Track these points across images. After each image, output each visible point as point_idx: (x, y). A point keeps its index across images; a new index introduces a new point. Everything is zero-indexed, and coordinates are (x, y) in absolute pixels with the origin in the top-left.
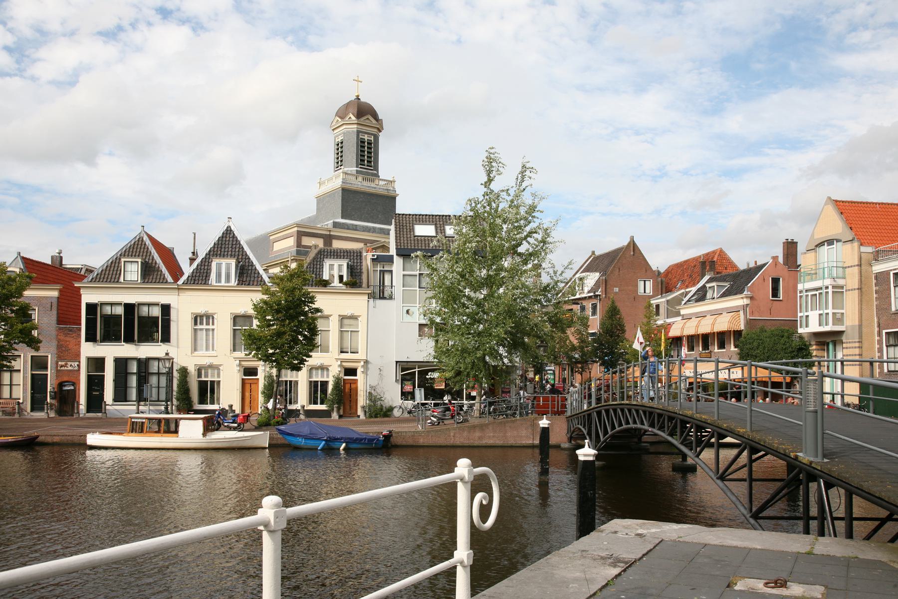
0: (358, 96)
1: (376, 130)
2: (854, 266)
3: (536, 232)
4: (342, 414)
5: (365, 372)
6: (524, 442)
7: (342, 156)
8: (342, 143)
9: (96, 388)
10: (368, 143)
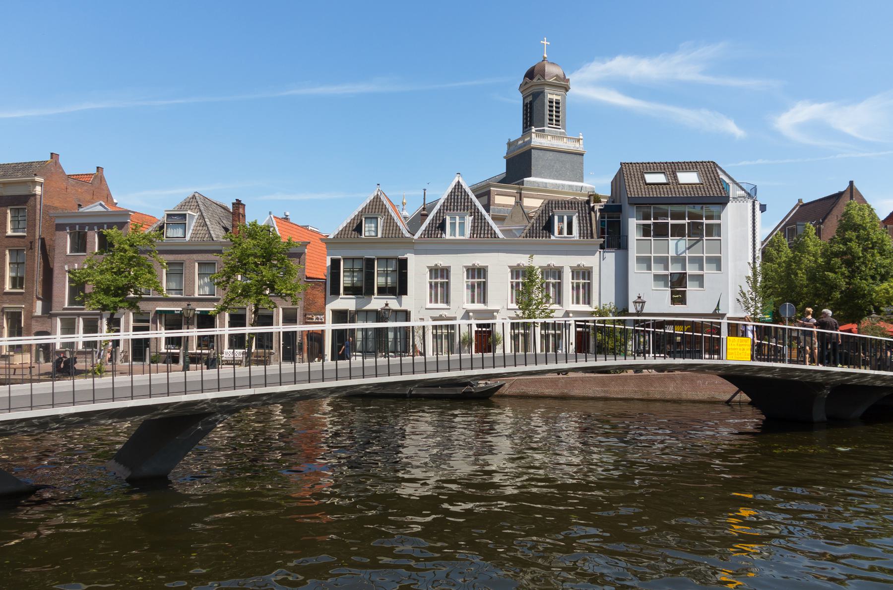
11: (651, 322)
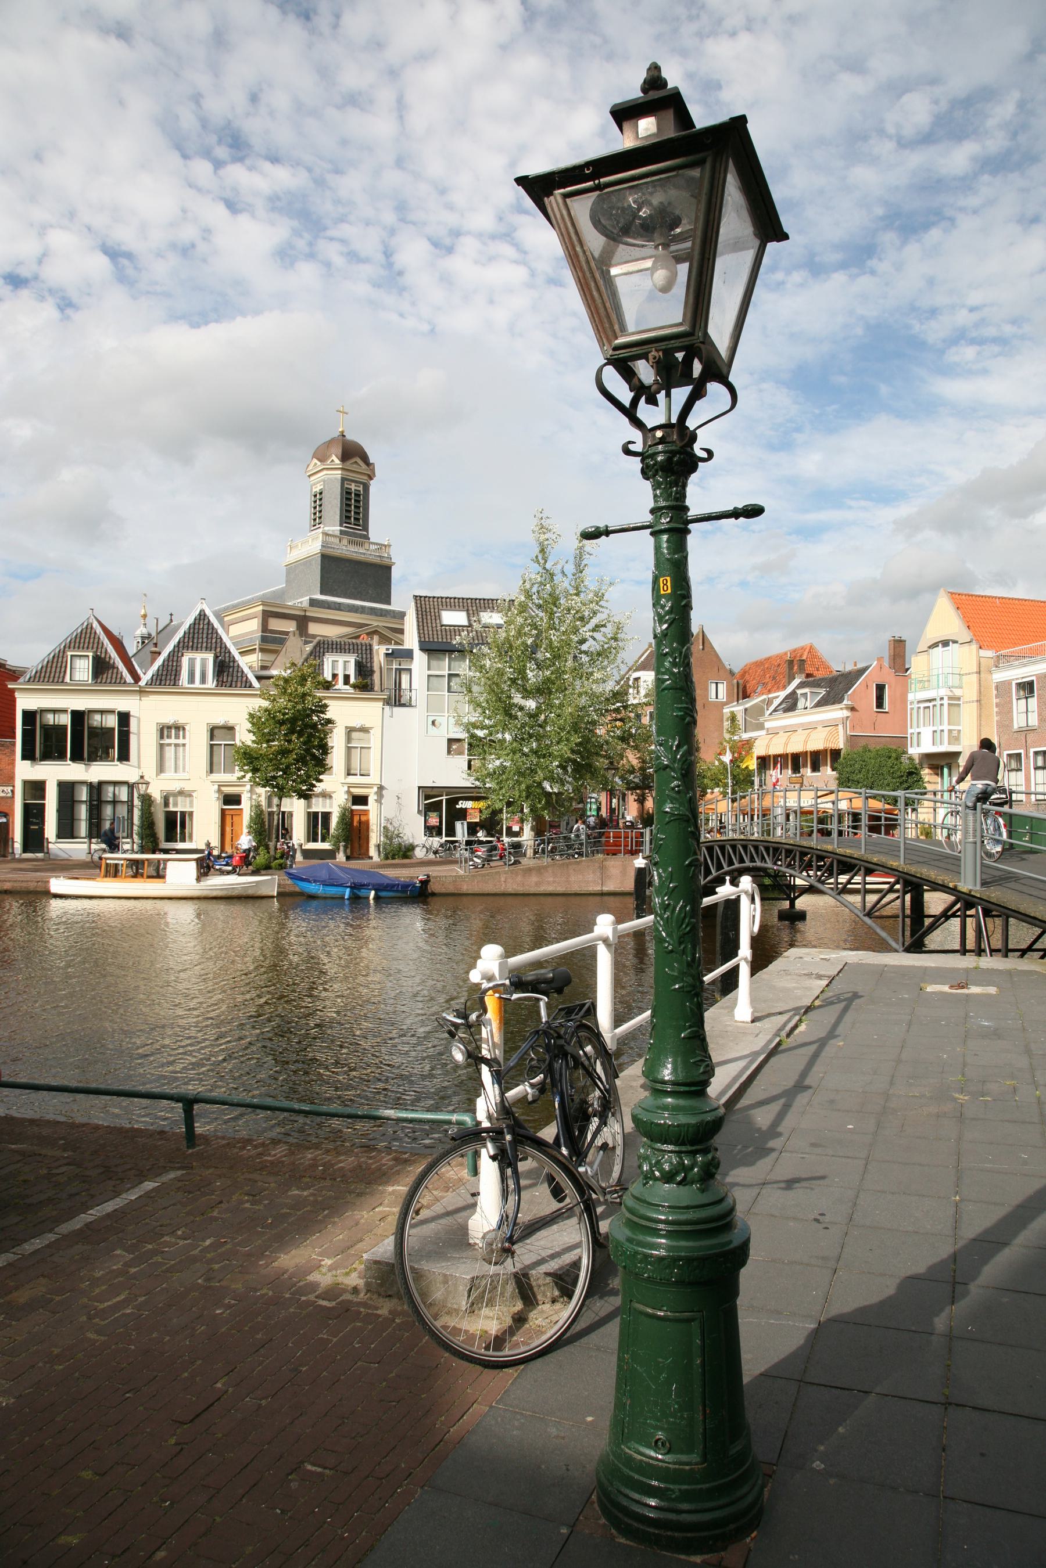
0: (342, 432)
1: (366, 478)
2: (973, 673)
3: (604, 626)
4: (349, 854)
5: (379, 800)
6: (591, 889)
7: (320, 512)
8: (321, 493)
9: (34, 820)
10: (355, 494)
11: (699, 857)
